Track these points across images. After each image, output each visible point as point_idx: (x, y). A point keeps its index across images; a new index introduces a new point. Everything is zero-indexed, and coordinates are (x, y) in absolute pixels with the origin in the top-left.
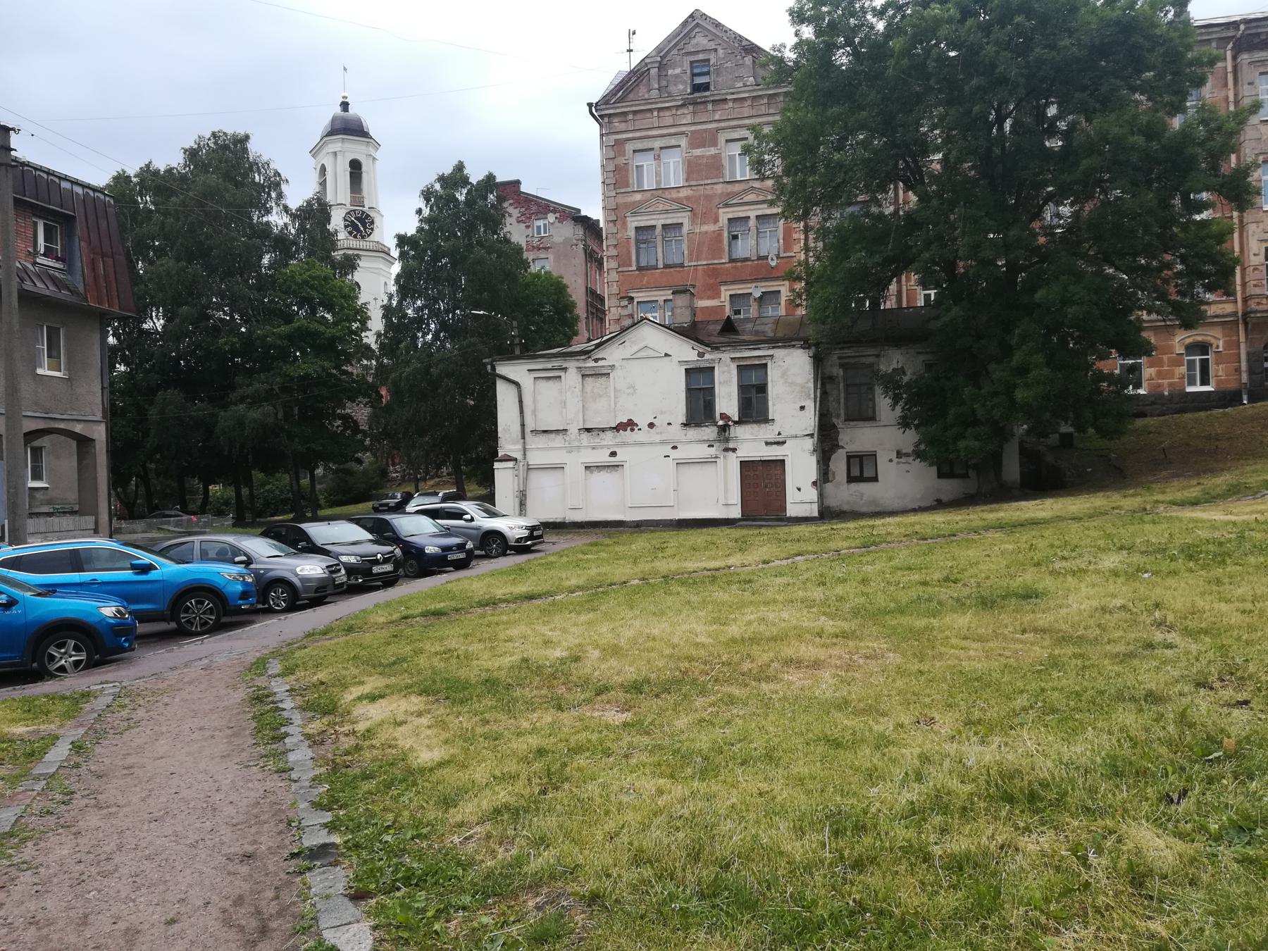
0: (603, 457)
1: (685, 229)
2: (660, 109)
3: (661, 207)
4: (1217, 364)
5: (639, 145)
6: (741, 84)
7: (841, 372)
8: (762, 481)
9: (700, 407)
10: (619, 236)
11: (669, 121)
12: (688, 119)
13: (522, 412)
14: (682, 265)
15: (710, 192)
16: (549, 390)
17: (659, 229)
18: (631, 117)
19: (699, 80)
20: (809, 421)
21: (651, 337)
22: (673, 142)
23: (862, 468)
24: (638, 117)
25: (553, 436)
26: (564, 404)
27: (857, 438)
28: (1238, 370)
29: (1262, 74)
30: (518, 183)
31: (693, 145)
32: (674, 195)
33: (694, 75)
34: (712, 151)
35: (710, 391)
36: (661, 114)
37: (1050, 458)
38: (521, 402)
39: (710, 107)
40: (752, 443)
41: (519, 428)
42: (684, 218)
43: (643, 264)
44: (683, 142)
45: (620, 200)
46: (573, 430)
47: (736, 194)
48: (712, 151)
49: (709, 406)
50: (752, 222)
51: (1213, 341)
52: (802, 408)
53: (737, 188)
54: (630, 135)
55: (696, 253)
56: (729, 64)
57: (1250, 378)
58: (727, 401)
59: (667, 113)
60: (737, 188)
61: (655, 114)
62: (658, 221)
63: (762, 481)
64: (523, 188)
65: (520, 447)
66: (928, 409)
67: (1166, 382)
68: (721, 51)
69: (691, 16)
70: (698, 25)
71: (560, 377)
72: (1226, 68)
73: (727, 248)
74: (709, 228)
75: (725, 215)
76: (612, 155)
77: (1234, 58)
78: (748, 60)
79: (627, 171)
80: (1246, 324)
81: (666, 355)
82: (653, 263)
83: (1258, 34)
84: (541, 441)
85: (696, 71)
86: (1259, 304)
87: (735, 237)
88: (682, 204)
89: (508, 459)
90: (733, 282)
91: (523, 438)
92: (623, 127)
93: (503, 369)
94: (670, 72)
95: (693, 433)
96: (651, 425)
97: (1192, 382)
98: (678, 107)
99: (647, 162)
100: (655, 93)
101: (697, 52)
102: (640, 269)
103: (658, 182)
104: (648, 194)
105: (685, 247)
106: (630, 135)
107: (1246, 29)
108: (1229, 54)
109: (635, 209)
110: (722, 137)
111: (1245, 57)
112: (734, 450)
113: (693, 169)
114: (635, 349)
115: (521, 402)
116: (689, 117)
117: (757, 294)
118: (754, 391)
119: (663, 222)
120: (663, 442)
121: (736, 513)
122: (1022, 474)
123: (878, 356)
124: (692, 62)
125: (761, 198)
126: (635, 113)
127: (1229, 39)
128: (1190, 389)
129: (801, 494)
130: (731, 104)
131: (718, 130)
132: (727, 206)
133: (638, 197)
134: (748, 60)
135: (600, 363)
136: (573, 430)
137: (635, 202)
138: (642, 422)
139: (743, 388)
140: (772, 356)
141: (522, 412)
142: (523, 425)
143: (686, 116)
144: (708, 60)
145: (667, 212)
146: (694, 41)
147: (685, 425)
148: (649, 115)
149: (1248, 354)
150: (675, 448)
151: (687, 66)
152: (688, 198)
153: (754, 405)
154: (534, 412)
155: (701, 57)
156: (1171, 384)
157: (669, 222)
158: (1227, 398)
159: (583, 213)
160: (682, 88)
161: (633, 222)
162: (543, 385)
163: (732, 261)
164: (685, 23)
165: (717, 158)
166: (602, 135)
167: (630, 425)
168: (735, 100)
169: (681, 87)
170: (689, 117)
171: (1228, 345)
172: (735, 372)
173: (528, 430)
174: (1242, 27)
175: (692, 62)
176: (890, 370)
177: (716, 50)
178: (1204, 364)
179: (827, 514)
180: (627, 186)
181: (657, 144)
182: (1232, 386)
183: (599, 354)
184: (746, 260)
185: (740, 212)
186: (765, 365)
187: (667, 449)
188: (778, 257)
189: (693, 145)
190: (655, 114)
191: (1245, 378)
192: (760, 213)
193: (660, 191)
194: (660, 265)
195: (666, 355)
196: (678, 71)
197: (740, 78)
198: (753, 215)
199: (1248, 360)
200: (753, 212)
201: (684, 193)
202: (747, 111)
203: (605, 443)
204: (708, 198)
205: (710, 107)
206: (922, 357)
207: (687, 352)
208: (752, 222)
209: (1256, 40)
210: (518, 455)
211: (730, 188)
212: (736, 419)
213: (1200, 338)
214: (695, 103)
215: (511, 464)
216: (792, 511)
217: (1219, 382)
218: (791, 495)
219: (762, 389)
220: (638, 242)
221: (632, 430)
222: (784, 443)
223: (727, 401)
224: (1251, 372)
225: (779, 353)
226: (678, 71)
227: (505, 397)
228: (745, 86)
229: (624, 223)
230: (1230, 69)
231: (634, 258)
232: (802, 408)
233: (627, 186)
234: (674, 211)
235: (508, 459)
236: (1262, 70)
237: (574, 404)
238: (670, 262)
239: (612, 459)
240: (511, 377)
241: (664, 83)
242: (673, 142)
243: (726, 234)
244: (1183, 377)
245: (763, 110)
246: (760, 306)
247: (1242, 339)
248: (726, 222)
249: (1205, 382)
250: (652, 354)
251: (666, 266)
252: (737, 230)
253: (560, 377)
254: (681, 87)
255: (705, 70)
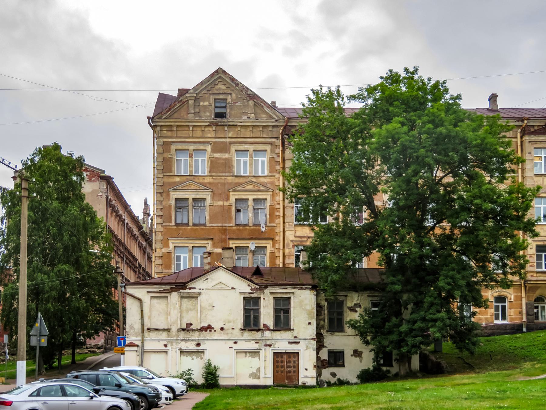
0: (191, 346)
1: (208, 202)
2: (194, 126)
3: (193, 187)
4: (510, 309)
5: (180, 147)
6: (246, 117)
7: (326, 304)
8: (286, 364)
9: (251, 322)
10: (164, 203)
11: (199, 134)
12: (212, 134)
13: (142, 317)
14: (204, 225)
15: (223, 181)
16: (159, 305)
17: (191, 201)
18: (175, 128)
19: (219, 111)
20: (312, 331)
21: (221, 276)
22: (201, 147)
23: (336, 359)
24: (180, 129)
25: (161, 332)
26: (168, 314)
27: (334, 342)
28: (521, 313)
29: (535, 148)
30: (57, 147)
31: (214, 151)
32: (201, 180)
33: (216, 107)
34: (226, 156)
35: (257, 311)
36: (195, 129)
37: (433, 358)
38: (142, 311)
39: (226, 128)
40: (282, 342)
41: (140, 327)
42: (207, 195)
43: (179, 221)
44: (209, 148)
45: (166, 180)
46: (174, 329)
47: (240, 184)
48: (226, 156)
49: (257, 319)
50: (250, 203)
51: (508, 295)
52: (310, 323)
53: (241, 180)
54: (174, 140)
55: (213, 218)
56: (239, 104)
57: (527, 318)
58: (267, 315)
59: (199, 129)
60: (241, 180)
61: (191, 128)
62: (191, 196)
63: (286, 364)
64: (64, 152)
65: (140, 338)
66: (374, 329)
67: (483, 317)
68: (234, 95)
69: (217, 71)
70: (220, 77)
71: (167, 297)
72: (517, 142)
73: (234, 217)
74: (227, 204)
75: (233, 196)
76: (161, 151)
77: (521, 137)
78: (251, 103)
79: (171, 162)
80: (525, 287)
81: (233, 288)
82: (185, 221)
83: (533, 126)
84: (153, 335)
85: (217, 105)
86: (532, 276)
87: (239, 211)
88: (206, 187)
89: (132, 345)
90: (238, 239)
91: (143, 332)
92: (169, 134)
93: (130, 290)
94: (201, 104)
95: (246, 334)
96: (222, 329)
97: (497, 318)
98: (206, 126)
99: (184, 158)
100: (191, 116)
101: (219, 94)
102: (177, 225)
103: (191, 171)
104: (185, 178)
105: (207, 214)
106: (174, 140)
107: (528, 122)
108: (519, 135)
109: (175, 186)
110: (233, 148)
111: (526, 138)
112: (270, 346)
113: (214, 165)
114: (214, 283)
115: (142, 311)
116: (213, 133)
117: (253, 248)
118: (282, 312)
119: (194, 197)
120: (229, 339)
121: (270, 382)
122: (420, 366)
123: (346, 296)
124: (215, 99)
125: (256, 188)
126: (178, 126)
127: (519, 127)
128: (496, 322)
129: (307, 372)
130: (239, 129)
131: (230, 143)
132: (235, 191)
133: (177, 179)
134: (251, 103)
135: (192, 291)
136: (174, 329)
137: (175, 182)
138: (217, 326)
139: (277, 311)
140: (293, 293)
141: (142, 317)
142: (143, 325)
143: (211, 132)
144: (226, 99)
145: (196, 190)
146: (217, 87)
147: (243, 330)
148: (187, 129)
149: (526, 304)
150: (236, 343)
151: (212, 101)
152: (210, 183)
153: (282, 321)
154: (150, 317)
155: (221, 97)
156: (486, 319)
157: (198, 197)
158: (516, 329)
159: (107, 174)
160: (209, 115)
161: (174, 195)
162: (155, 301)
163: (237, 225)
164: (212, 75)
165: (230, 160)
166: (154, 137)
167: (209, 328)
168: (242, 126)
169: (208, 114)
170: (213, 133)
171: (516, 298)
172: (272, 301)
173: (145, 328)
174: (526, 122)
175: (215, 99)
176: (353, 305)
177: (231, 94)
178: (504, 308)
179: (320, 384)
180: (171, 172)
181: (192, 147)
182: (518, 321)
183: (191, 285)
184: (246, 225)
185: (243, 195)
186: (290, 298)
187: (231, 344)
188: (266, 226)
189: (214, 151)
190: (191, 128)
191: (525, 319)
192: (255, 197)
193: (192, 177)
194: (191, 224)
195: (233, 288)
196: (206, 104)
197: (245, 113)
198: (251, 198)
199: (527, 307)
200: (251, 197)
201: (207, 180)
202: (248, 134)
203: (193, 338)
204: (224, 184)
205: (226, 128)
206: (370, 299)
207: (244, 287)
208: (250, 203)
209: (532, 130)
210: (139, 343)
211: (237, 180)
212: (272, 328)
213: (502, 294)
214: (217, 125)
215: (135, 348)
216: (301, 381)
217: (511, 319)
218: (302, 373)
219: (287, 311)
220: (176, 207)
221: (210, 331)
222: (299, 343)
223: (267, 315)
224: (528, 314)
225: (297, 292)
226: (206, 104)
227: (132, 307)
228: (249, 118)
229: (168, 195)
230: (519, 143)
231: (173, 218)
232: (310, 323)
233: (171, 172)
234: (203, 190)
235: (132, 345)
236: (536, 146)
237: (174, 314)
238: (197, 222)
239: (198, 348)
240: (137, 295)
241: (197, 110)
242: (201, 147)
243: (233, 208)
244: (492, 315)
245: (259, 134)
246: (254, 255)
247: (523, 295)
248: (234, 200)
249: (504, 318)
250: (224, 287)
251: (194, 225)
252: (241, 206)
253: (167, 297)
254: (208, 114)
255: (223, 105)
